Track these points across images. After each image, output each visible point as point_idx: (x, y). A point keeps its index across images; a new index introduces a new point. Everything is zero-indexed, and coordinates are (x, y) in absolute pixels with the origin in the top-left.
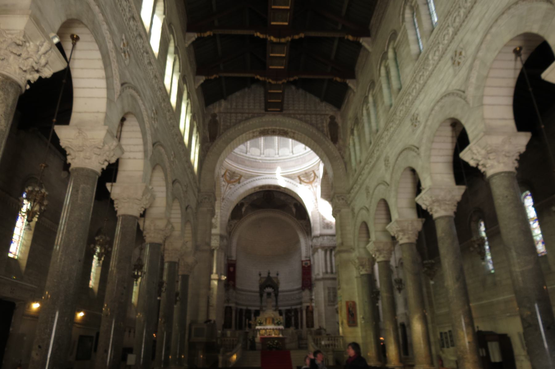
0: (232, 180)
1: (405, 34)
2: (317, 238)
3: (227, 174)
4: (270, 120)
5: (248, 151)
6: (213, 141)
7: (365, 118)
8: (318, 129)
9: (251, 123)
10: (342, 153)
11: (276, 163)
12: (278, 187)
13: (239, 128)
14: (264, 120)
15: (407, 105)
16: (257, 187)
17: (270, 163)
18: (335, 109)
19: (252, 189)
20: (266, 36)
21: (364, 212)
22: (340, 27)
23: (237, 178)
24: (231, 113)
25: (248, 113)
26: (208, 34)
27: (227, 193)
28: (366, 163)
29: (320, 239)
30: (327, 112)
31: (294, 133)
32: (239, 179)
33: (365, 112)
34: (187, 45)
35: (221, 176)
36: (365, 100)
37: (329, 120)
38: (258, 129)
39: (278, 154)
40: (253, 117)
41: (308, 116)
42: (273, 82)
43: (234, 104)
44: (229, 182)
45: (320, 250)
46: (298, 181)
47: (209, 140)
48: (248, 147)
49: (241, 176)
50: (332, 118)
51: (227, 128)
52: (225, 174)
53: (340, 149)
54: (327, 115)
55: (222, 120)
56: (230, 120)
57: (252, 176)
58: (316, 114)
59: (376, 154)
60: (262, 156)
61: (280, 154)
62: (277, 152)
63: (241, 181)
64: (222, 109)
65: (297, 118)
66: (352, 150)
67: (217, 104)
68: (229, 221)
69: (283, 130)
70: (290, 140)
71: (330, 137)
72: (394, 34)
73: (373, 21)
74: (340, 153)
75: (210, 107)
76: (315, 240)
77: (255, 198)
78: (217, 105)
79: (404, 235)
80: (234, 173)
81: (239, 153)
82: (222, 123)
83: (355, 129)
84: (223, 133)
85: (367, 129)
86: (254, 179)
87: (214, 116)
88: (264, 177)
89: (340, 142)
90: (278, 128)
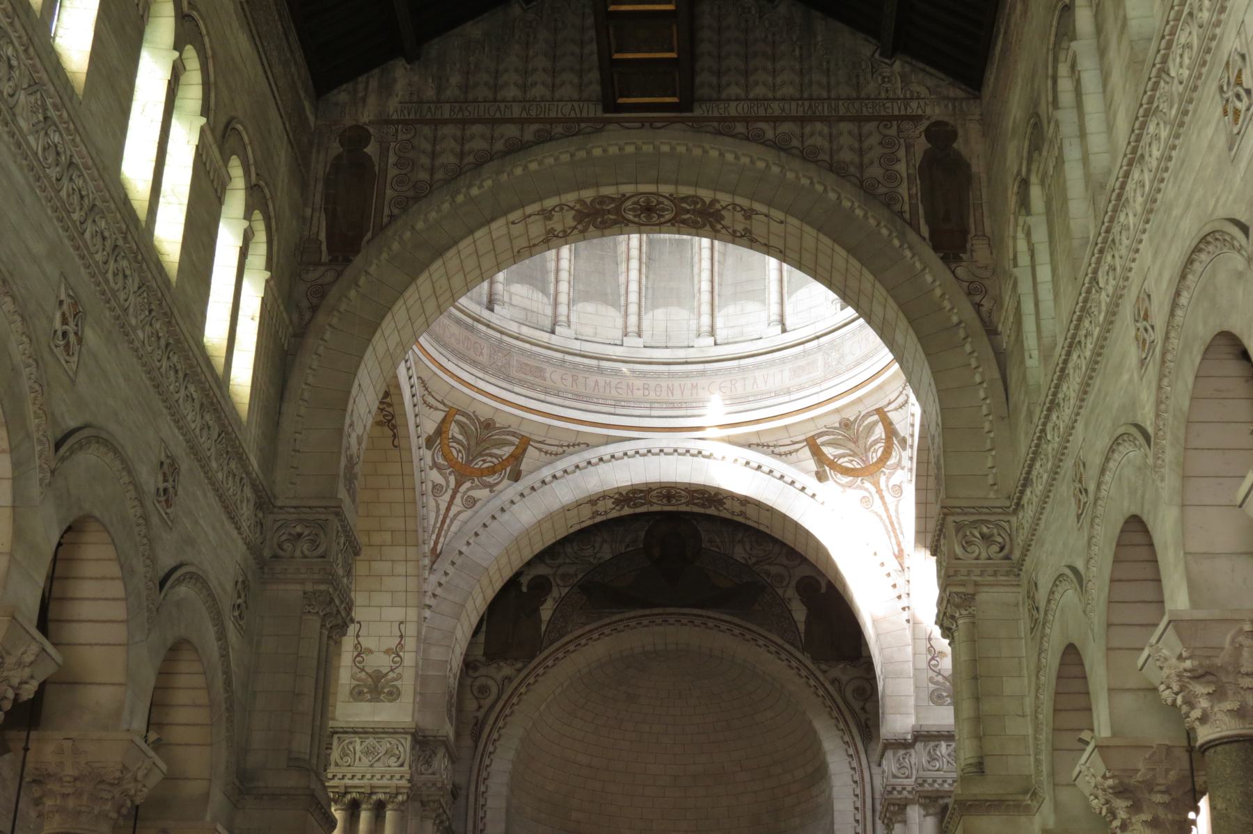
0: (479, 464)
2: (901, 752)
3: (454, 430)
5: (563, 318)
6: (348, 261)
7: (1067, 117)
8: (867, 190)
9: (533, 166)
10: (987, 304)
11: (703, 373)
12: (711, 497)
13: (475, 191)
15: (1205, 15)
16: (604, 496)
17: (672, 375)
18: (956, 92)
19: (578, 504)
21: (1069, 595)
23: (506, 451)
25: (521, 122)
27: (454, 529)
28: (1073, 344)
29: (918, 756)
31: (749, 214)
32: (517, 457)
33: (1065, 85)
35: (422, 441)
36: (1065, 31)
37: (922, 145)
38: (570, 198)
39: (712, 333)
40: (543, 138)
41: (818, 126)
43: (455, 79)
44: (463, 473)
45: (914, 812)
46: (812, 465)
47: (325, 257)
48: (563, 298)
49: (525, 442)
51: (419, 194)
52: (440, 431)
53: (975, 290)
54: (916, 119)
55: (392, 159)
56: (434, 155)
57: (580, 444)
58: (859, 119)
59: (1108, 284)
60: (632, 341)
61: (721, 334)
62: (705, 320)
63: (523, 467)
64: (393, 105)
65: (759, 139)
66: (1025, 287)
68: (469, 665)
69: (694, 200)
70: (773, 262)
71: (925, 231)
74: (978, 306)
75: (341, 96)
76: (890, 764)
77: (606, 553)
79: (1218, 695)
80: (488, 425)
81: (513, 327)
82: (393, 172)
83: (1034, 179)
84: (392, 217)
85: (1074, 173)
86: (592, 455)
87: (357, 137)
88: (641, 446)
89: (980, 251)
90: (666, 189)
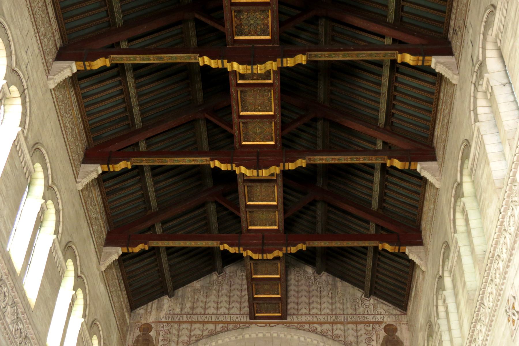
1: (482, 145)
4: (260, 335)
7: (442, 322)
14: (247, 336)
15: (497, 281)
20: (232, 167)
22: (379, 146)
24: (180, 323)
25: (215, 323)
26: (121, 166)
30: (379, 318)
33: (441, 309)
34: (80, 187)
40: (224, 330)
42: (255, 256)
43: (189, 305)
50: (390, 330)
54: (380, 323)
55: (161, 338)
58: (356, 323)
65: (315, 331)
67: (154, 304)
72: (468, 145)
73: (437, 132)
75: (141, 311)
78: (155, 306)
87: (146, 328)
